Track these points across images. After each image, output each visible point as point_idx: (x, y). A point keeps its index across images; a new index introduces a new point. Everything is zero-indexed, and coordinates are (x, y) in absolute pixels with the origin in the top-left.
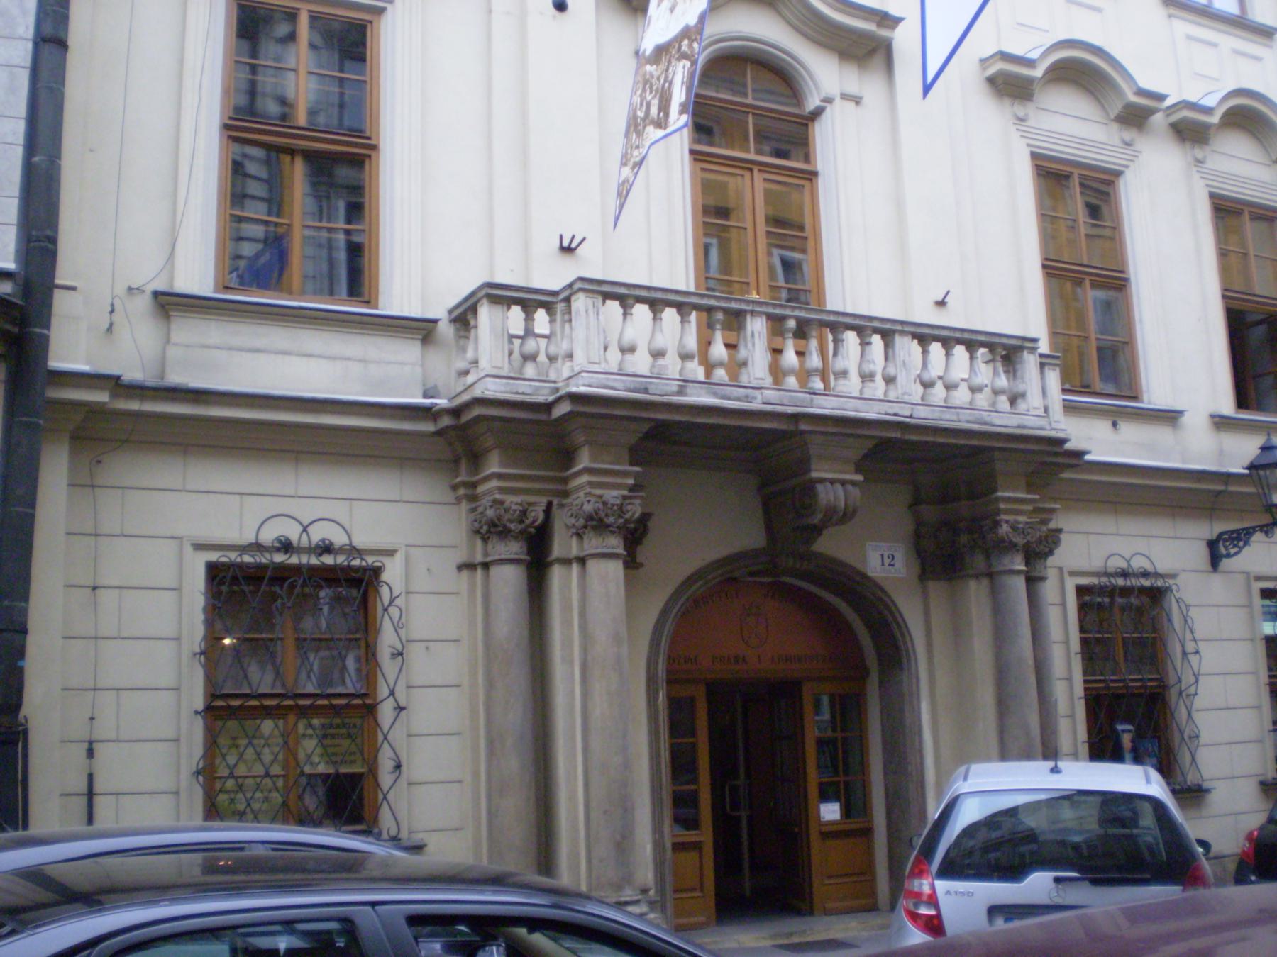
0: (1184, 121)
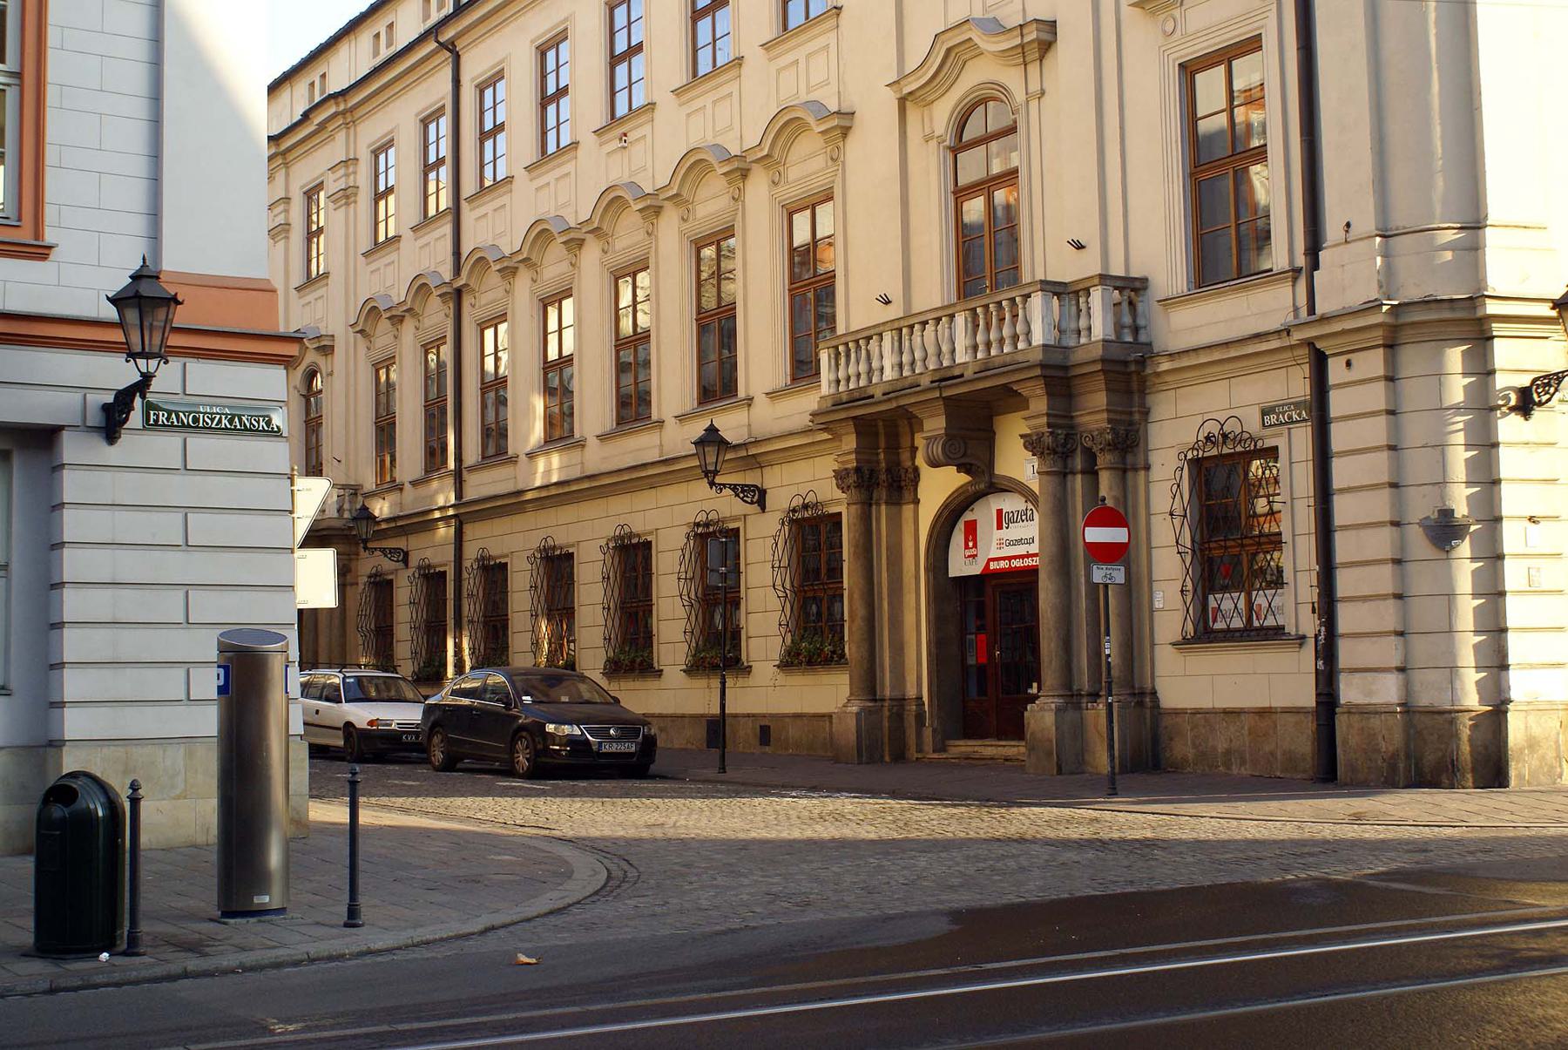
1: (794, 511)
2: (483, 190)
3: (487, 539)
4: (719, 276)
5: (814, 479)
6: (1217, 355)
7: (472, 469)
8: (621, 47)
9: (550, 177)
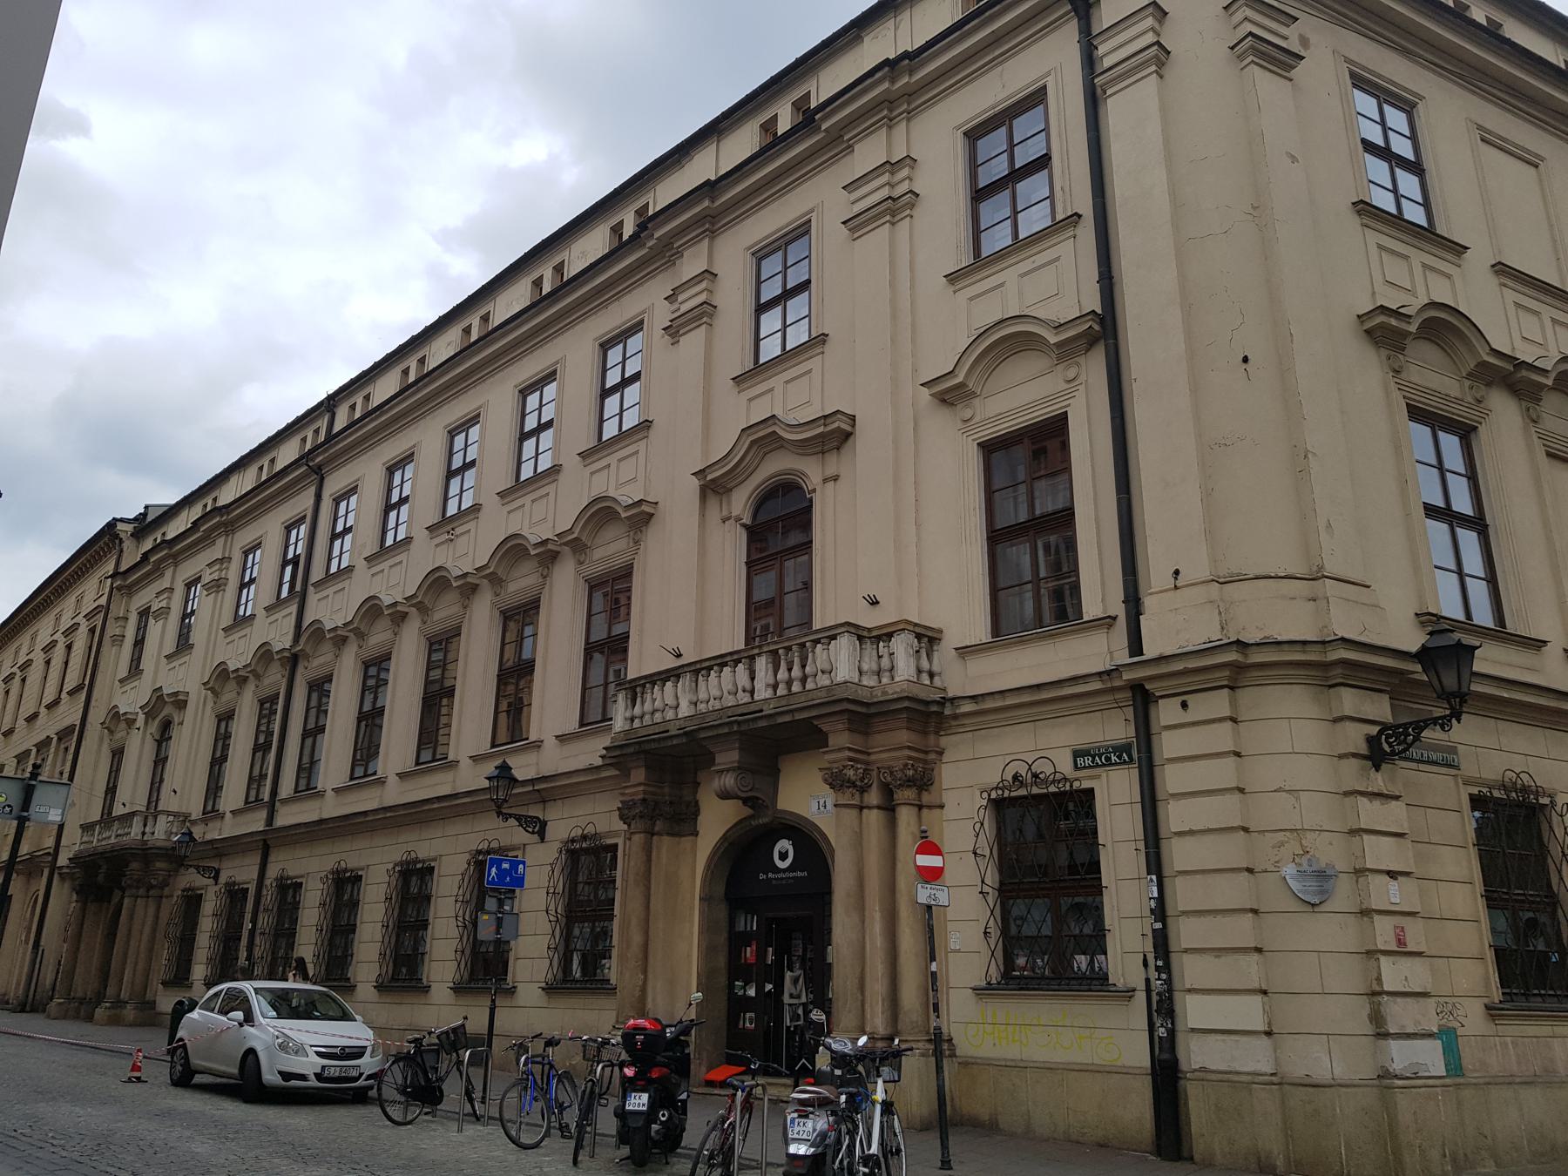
0: (1382, 326)
1: (573, 841)
2: (329, 578)
3: (284, 863)
4: (444, 666)
5: (598, 816)
6: (1026, 698)
7: (285, 801)
8: (457, 462)
9: (385, 565)
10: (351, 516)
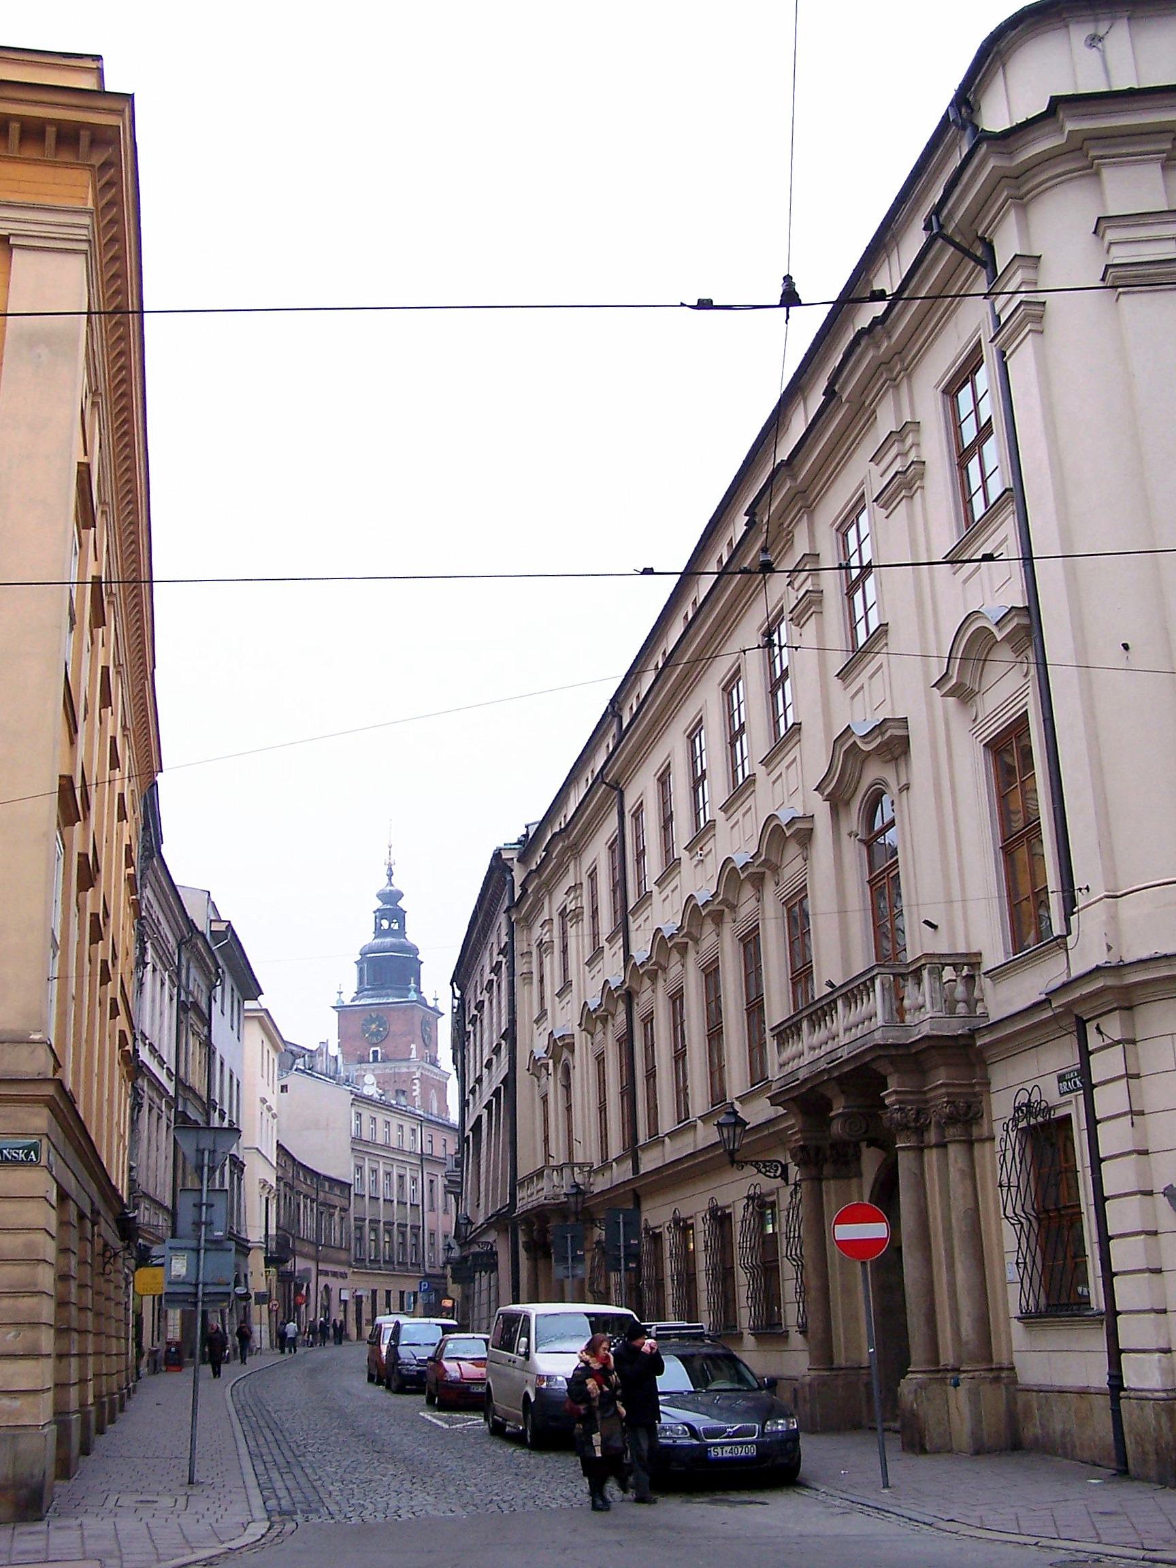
3: (657, 1214)
10: (866, 547)
